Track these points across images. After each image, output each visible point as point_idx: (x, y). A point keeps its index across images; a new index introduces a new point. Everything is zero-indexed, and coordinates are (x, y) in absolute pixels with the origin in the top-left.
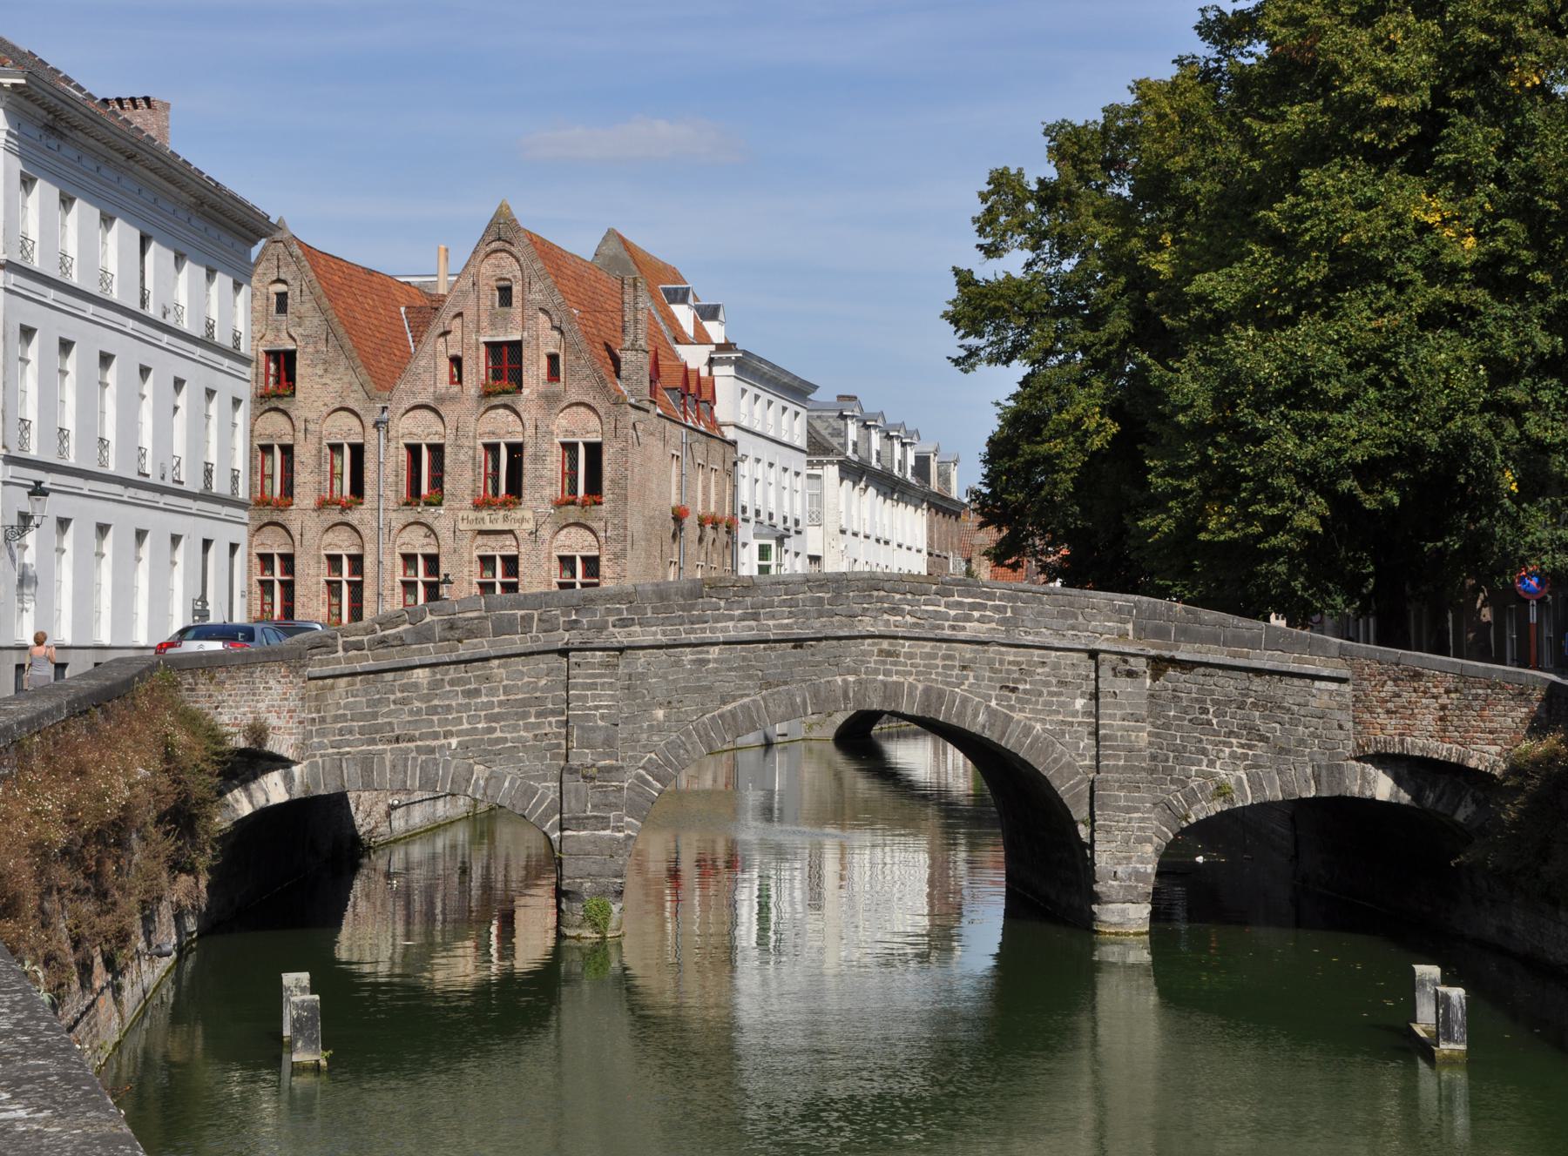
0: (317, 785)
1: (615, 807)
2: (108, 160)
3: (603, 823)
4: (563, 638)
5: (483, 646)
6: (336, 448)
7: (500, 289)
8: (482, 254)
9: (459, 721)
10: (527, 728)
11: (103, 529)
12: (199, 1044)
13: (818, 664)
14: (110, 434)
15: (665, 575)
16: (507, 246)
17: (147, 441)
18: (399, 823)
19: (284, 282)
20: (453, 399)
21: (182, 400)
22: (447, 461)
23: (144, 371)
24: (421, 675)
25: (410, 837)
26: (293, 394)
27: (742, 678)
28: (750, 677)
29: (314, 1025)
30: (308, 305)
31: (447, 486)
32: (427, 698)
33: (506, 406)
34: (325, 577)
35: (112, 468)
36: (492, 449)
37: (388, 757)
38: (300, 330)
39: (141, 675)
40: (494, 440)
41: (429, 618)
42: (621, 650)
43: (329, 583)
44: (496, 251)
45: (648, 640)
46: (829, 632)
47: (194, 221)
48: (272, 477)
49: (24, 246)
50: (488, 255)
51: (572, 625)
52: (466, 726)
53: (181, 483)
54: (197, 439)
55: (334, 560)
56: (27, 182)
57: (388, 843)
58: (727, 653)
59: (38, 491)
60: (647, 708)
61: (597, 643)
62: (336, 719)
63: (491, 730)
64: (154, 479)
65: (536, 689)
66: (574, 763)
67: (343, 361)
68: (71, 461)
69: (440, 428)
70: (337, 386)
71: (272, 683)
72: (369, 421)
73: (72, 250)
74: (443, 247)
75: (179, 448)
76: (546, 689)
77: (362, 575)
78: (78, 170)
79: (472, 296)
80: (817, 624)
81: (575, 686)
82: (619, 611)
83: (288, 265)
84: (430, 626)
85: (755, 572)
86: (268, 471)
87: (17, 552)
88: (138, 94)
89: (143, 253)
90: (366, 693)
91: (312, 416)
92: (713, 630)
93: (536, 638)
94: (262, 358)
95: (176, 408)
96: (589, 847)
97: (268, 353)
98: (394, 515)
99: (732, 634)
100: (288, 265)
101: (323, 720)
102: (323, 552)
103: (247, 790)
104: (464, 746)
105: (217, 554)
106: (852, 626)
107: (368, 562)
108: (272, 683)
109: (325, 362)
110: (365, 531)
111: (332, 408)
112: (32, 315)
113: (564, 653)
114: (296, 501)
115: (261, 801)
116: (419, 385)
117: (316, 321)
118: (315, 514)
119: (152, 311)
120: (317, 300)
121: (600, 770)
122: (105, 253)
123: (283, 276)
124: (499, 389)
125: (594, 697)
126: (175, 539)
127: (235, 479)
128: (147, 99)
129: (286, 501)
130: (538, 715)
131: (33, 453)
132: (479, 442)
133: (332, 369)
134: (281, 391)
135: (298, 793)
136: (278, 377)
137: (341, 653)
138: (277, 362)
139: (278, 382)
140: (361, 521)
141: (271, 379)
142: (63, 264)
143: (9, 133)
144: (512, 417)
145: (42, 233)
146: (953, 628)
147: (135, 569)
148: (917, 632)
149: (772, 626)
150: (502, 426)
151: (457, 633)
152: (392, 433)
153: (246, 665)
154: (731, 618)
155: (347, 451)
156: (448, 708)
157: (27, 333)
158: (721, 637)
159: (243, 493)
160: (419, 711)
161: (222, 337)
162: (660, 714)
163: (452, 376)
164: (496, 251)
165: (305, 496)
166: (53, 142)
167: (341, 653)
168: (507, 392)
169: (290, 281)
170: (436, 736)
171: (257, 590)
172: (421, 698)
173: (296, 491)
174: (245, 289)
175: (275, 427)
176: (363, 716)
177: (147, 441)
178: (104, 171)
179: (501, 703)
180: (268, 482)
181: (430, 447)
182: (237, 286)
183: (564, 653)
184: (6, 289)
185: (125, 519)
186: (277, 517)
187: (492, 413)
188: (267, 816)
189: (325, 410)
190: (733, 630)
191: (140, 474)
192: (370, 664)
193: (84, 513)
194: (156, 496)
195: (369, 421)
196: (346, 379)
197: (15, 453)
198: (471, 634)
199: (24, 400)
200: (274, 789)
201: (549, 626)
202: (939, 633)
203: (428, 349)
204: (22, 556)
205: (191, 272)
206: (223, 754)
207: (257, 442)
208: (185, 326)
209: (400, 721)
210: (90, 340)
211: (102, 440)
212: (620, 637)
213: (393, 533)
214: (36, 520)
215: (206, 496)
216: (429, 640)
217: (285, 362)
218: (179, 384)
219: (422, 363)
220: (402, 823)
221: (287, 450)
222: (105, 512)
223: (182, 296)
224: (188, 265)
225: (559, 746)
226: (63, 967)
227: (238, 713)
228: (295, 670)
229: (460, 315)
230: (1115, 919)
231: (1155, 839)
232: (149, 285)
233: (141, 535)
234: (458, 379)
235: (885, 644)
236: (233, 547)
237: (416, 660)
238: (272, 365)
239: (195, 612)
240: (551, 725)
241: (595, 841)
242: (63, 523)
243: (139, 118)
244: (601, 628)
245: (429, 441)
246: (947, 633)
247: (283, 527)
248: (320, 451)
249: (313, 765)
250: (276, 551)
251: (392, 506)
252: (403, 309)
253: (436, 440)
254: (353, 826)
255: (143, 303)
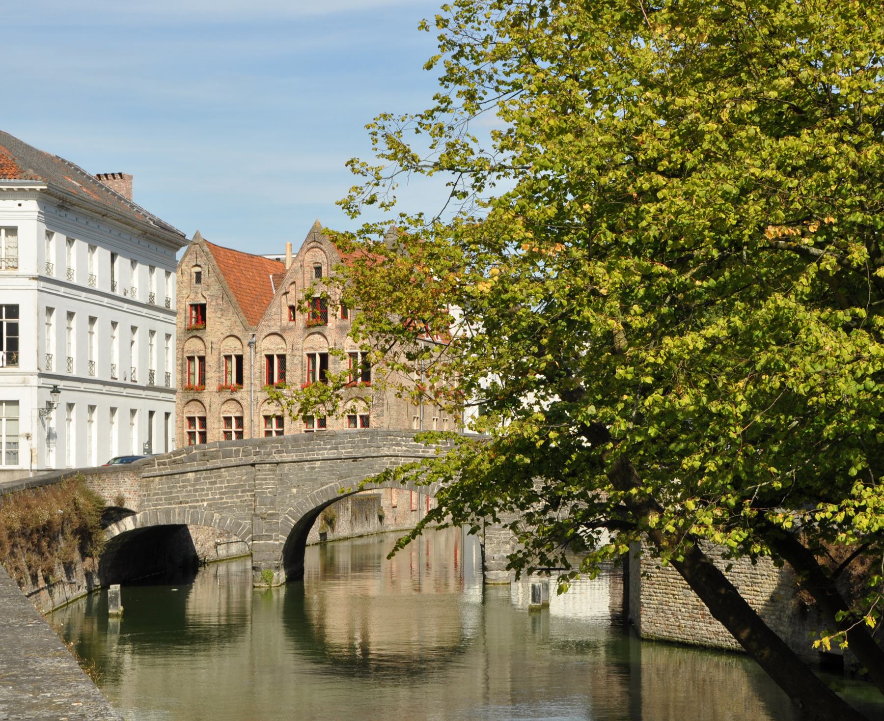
0: (147, 522)
1: (275, 531)
2: (92, 218)
3: (270, 537)
4: (254, 459)
5: (218, 463)
6: (228, 358)
7: (316, 268)
8: (305, 249)
9: (207, 495)
10: (238, 497)
11: (92, 408)
12: (95, 626)
13: (363, 468)
14: (95, 359)
15: (410, 425)
16: (319, 245)
17: (116, 360)
18: (222, 551)
19: (199, 266)
20: (291, 329)
21: (136, 338)
22: (287, 364)
23: (114, 324)
24: (191, 476)
25: (230, 559)
26: (205, 328)
27: (330, 475)
28: (334, 474)
29: (117, 600)
30: (213, 279)
31: (287, 378)
32: (193, 485)
33: (319, 333)
34: (223, 429)
35: (96, 376)
36: (312, 356)
37: (177, 510)
38: (208, 293)
39: (66, 477)
40: (312, 352)
41: (194, 451)
42: (277, 463)
43: (225, 432)
44: (313, 248)
45: (290, 459)
46: (368, 455)
47: (141, 243)
48: (194, 374)
49: (48, 267)
50: (308, 250)
51: (257, 453)
52: (210, 497)
53: (135, 381)
54: (144, 357)
55: (228, 420)
56: (49, 235)
57: (215, 562)
58: (324, 464)
59: (55, 390)
60: (289, 488)
61: (267, 460)
62: (155, 494)
63: (222, 498)
64: (120, 380)
65: (241, 481)
66: (258, 512)
67: (231, 309)
68: (74, 373)
69: (284, 346)
70: (227, 323)
71: (126, 480)
72: (246, 342)
73: (74, 266)
74: (289, 243)
75: (135, 363)
76: (246, 480)
77: (242, 427)
78: (76, 225)
79: (301, 272)
80: (363, 451)
81: (258, 479)
82: (277, 447)
83: (201, 257)
84: (195, 455)
85: (263, 435)
86: (192, 371)
87: (46, 422)
88: (116, 172)
89: (113, 261)
90: (167, 483)
91: (215, 340)
92: (318, 454)
93: (241, 459)
94: (188, 308)
95: (132, 343)
96: (264, 548)
97: (191, 305)
98: (259, 394)
99: (326, 456)
100: (201, 257)
101: (149, 495)
102: (222, 416)
103: (117, 524)
104: (210, 505)
105: (158, 419)
106: (378, 452)
107: (246, 421)
108: (126, 480)
109: (222, 310)
110: (244, 403)
111: (226, 335)
112: (51, 301)
113: (253, 465)
114: (207, 387)
115: (123, 529)
116: (272, 322)
117: (217, 288)
118: (217, 394)
119: (118, 292)
120: (217, 276)
121: (268, 515)
122: (92, 265)
123: (199, 263)
124: (315, 323)
125: (266, 484)
126: (133, 412)
127: (167, 377)
128: (120, 174)
129: (201, 387)
130: (242, 492)
131: (54, 371)
132: (305, 353)
133: (225, 314)
134: (199, 327)
135: (139, 526)
136: (197, 318)
137: (156, 467)
138: (196, 310)
139: (197, 322)
140: (242, 398)
141: (193, 320)
142: (68, 274)
143: (39, 213)
144: (322, 339)
145: (57, 259)
146: (423, 452)
147: (111, 428)
148: (407, 454)
149: (343, 452)
150: (318, 344)
151: (207, 458)
152: (258, 349)
153: (115, 472)
154: (326, 449)
155: (234, 359)
156: (203, 490)
157: (50, 310)
158: (321, 457)
159: (172, 385)
160: (190, 491)
161: (159, 302)
162: (294, 491)
163: (290, 317)
164: (313, 248)
165: (212, 384)
166: (63, 213)
167: (156, 467)
168: (320, 325)
169: (203, 265)
170: (197, 501)
171: (187, 437)
172: (190, 486)
173: (207, 382)
174: (173, 274)
175: (194, 346)
176: (166, 493)
177: (116, 360)
178: (90, 224)
179: (226, 487)
180: (192, 377)
181: (279, 356)
182: (168, 274)
183: (253, 465)
184: (39, 290)
185: (103, 402)
186: (197, 396)
187: (311, 337)
188: (125, 535)
189: (222, 337)
190: (326, 454)
191: (112, 378)
192: (169, 471)
193: (82, 400)
194: (122, 389)
195: (246, 342)
196: (233, 319)
197: (44, 371)
198: (213, 458)
199: (49, 344)
200: (128, 524)
201: (247, 454)
202: (417, 454)
203: (277, 302)
204: (49, 423)
205: (141, 269)
206: (102, 508)
207: (186, 355)
208: (137, 299)
209: (182, 496)
210: (83, 311)
211: (91, 361)
212: (277, 458)
213: (259, 404)
214: (55, 406)
215: (151, 388)
216: (194, 460)
217: (200, 310)
218: (134, 329)
219: (274, 310)
220: (225, 552)
221: (202, 359)
222: (93, 399)
223: (135, 282)
224: (138, 266)
225: (251, 505)
226: (22, 572)
227: (112, 492)
228: (137, 474)
229: (294, 283)
230: (493, 577)
231: (512, 542)
232: (116, 279)
233: (113, 410)
234: (293, 318)
235: (393, 459)
236: (167, 415)
237: (189, 469)
238: (194, 313)
239: (145, 450)
240: (248, 496)
241: (266, 545)
242: (70, 406)
243: (114, 185)
244: (270, 454)
245: (278, 353)
246: (421, 454)
247: (200, 402)
248: (219, 359)
249: (145, 514)
250: (197, 415)
251: (259, 389)
252: (271, 276)
253: (281, 352)
254: (195, 551)
255: (113, 289)
